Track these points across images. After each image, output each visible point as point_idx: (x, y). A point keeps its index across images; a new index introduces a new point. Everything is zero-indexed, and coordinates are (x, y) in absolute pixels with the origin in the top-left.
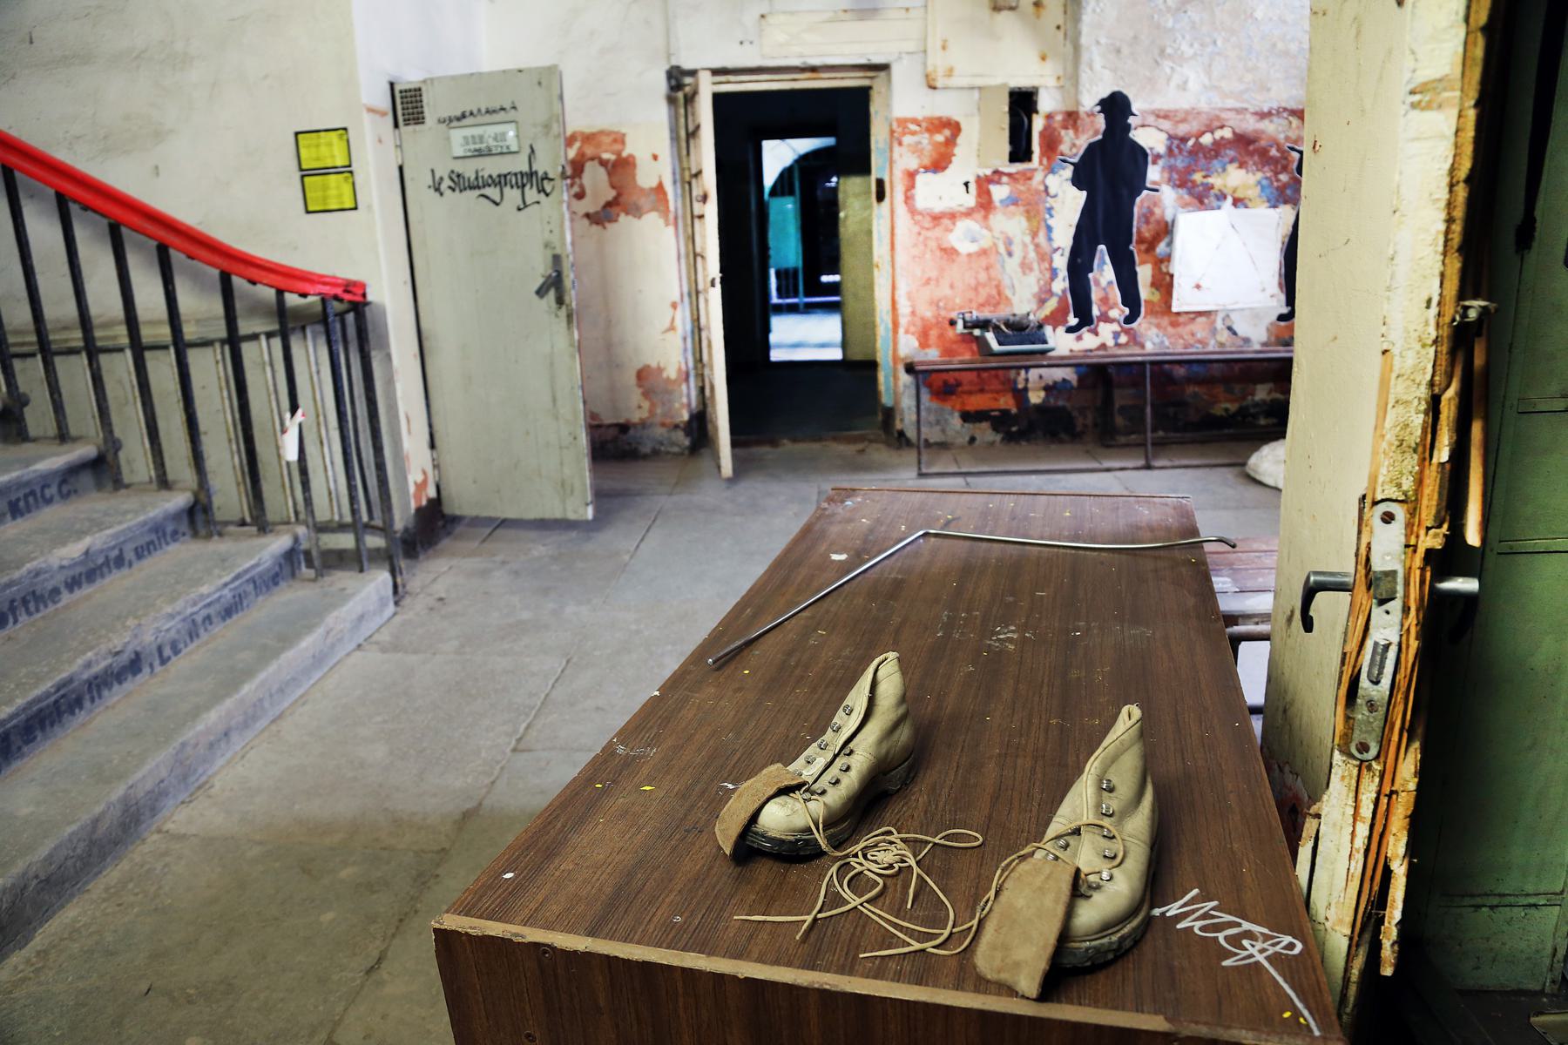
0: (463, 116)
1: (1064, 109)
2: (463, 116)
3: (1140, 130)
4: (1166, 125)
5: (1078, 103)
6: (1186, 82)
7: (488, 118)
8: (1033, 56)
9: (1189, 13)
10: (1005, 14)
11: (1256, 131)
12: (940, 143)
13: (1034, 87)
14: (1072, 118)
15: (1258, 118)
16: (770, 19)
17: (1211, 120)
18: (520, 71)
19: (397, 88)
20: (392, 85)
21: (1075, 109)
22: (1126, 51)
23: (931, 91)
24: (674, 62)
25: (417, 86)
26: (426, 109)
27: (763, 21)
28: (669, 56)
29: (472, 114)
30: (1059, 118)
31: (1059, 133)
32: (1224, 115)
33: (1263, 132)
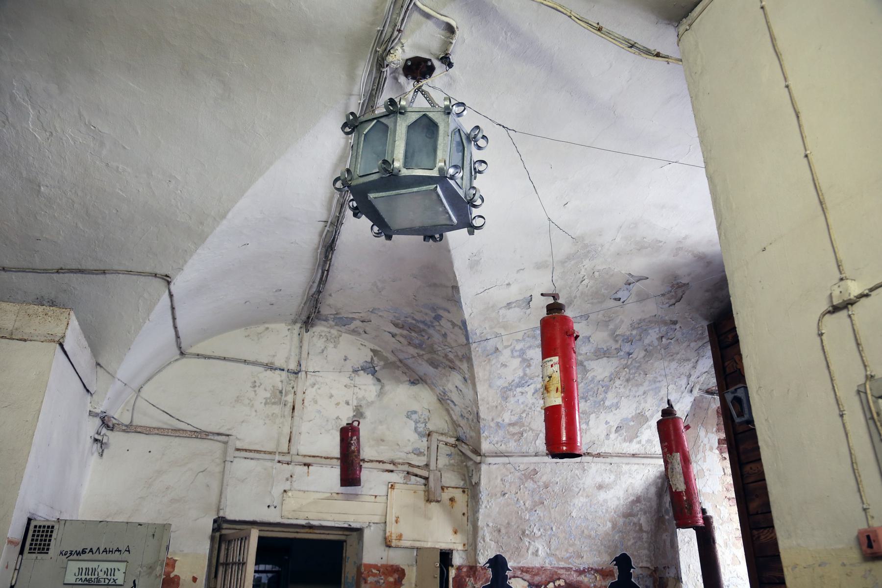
0: (84, 552)
1: (468, 564)
2: (84, 552)
3: (513, 580)
4: (527, 576)
5: (476, 561)
6: (537, 551)
7: (104, 556)
8: (449, 531)
9: (537, 512)
10: (433, 504)
11: (578, 582)
12: (391, 583)
13: (450, 550)
14: (473, 569)
15: (578, 574)
16: (290, 494)
17: (553, 575)
18: (140, 525)
19: (33, 524)
20: (29, 520)
21: (474, 564)
22: (503, 531)
23: (387, 549)
24: (221, 514)
25: (50, 524)
26: (53, 543)
27: (285, 495)
28: (218, 510)
29: (91, 550)
30: (465, 570)
31: (465, 580)
32: (559, 572)
33: (582, 582)
